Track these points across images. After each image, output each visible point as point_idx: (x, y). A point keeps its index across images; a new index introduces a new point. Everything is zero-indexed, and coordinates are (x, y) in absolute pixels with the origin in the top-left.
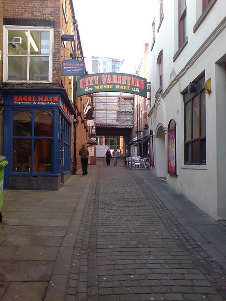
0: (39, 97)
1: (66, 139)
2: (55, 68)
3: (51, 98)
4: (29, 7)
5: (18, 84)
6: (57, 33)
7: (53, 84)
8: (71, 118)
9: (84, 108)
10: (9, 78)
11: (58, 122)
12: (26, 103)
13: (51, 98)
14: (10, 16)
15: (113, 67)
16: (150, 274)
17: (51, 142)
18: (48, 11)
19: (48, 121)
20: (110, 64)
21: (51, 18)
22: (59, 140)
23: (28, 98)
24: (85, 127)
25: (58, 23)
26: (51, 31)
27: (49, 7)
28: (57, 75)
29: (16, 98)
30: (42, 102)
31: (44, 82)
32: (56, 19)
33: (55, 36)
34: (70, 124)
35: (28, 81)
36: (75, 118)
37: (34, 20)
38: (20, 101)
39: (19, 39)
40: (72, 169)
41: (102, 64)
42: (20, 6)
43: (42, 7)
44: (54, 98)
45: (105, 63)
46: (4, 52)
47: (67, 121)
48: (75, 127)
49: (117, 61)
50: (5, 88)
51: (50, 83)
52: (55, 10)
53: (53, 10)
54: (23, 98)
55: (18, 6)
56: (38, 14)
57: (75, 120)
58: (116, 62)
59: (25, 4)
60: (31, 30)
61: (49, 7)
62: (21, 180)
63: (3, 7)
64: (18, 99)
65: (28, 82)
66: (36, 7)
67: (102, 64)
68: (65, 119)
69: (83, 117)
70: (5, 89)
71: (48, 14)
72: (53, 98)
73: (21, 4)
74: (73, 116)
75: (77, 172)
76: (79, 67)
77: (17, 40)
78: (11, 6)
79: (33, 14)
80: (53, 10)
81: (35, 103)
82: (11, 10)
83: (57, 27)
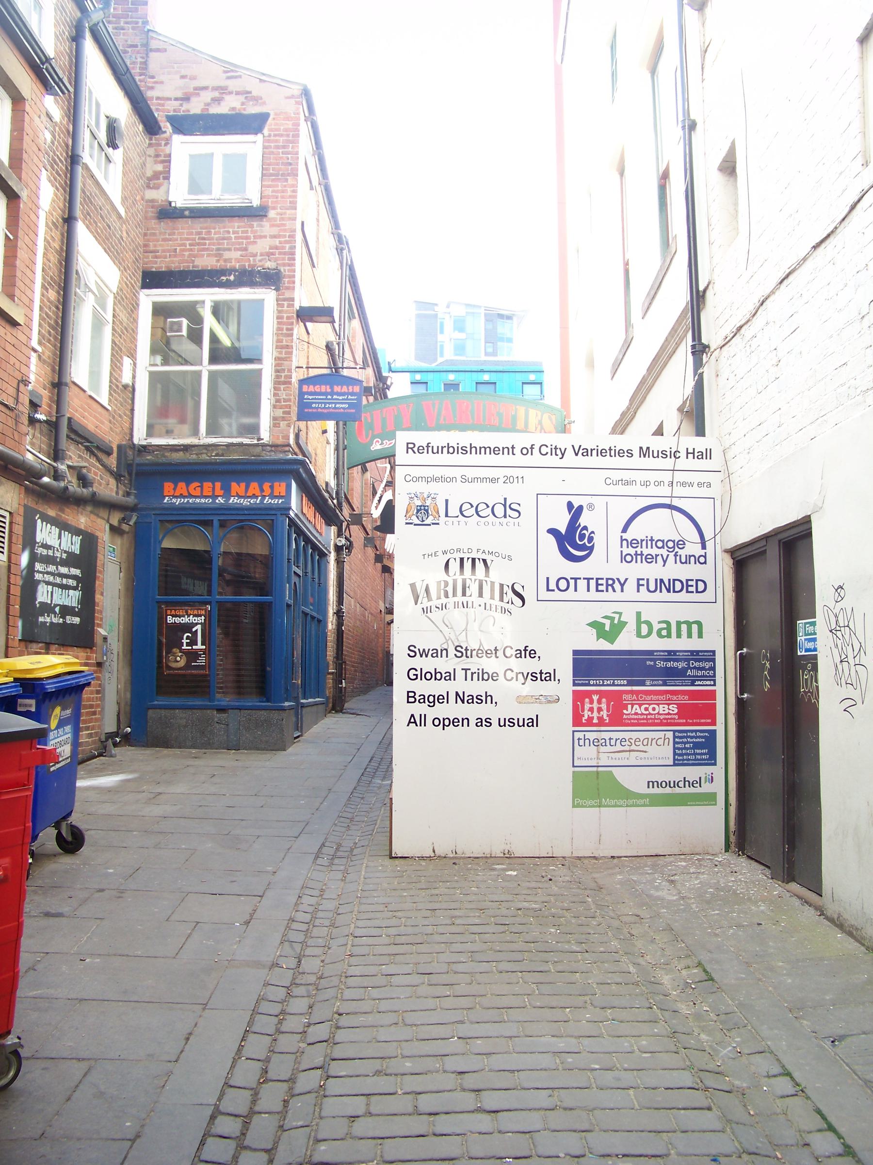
0: (234, 484)
1: (311, 600)
2: (278, 401)
3: (266, 486)
4: (212, 239)
5: (174, 448)
6: (286, 303)
7: (271, 446)
8: (328, 537)
9: (374, 493)
10: (151, 430)
11: (290, 547)
12: (198, 500)
13: (266, 486)
14: (160, 265)
15: (492, 338)
16: (674, 1132)
17: (263, 613)
18: (263, 246)
19: (259, 548)
20: (477, 326)
21: (270, 264)
22: (288, 606)
23: (202, 487)
24: (379, 558)
25: (290, 277)
26: (268, 296)
27: (265, 237)
28: (283, 419)
29: (168, 486)
30: (240, 497)
31: (246, 441)
32: (284, 265)
33: (279, 312)
34: (323, 555)
35: (204, 439)
36: (339, 534)
37: (223, 272)
38: (182, 496)
39: (180, 324)
40: (329, 691)
41: (449, 326)
42: (188, 239)
43: (247, 238)
44: (276, 484)
45: (459, 325)
46: (138, 362)
47: (315, 547)
48: (340, 563)
49: (501, 316)
50: (138, 460)
51: (264, 445)
52: (280, 243)
53: (277, 242)
54: (187, 486)
55: (181, 239)
56: (235, 255)
57: (342, 542)
58: (500, 322)
59: (199, 233)
60: (222, 518)
61: (265, 237)
62: (183, 722)
63: (145, 246)
64: (175, 489)
65: (202, 442)
66: (230, 238)
67: (449, 326)
68: (308, 540)
69: (369, 527)
70: (138, 465)
71: (262, 255)
72: (272, 487)
73: (192, 234)
74: (333, 529)
75: (346, 705)
76: (348, 394)
77: (175, 327)
78: (164, 240)
79: (220, 255)
80: (277, 242)
81: (220, 500)
82: (164, 251)
83: (288, 288)
